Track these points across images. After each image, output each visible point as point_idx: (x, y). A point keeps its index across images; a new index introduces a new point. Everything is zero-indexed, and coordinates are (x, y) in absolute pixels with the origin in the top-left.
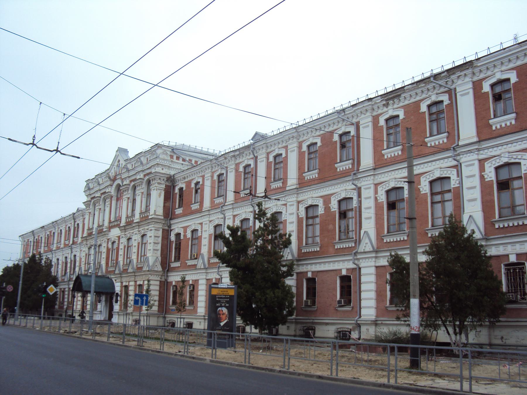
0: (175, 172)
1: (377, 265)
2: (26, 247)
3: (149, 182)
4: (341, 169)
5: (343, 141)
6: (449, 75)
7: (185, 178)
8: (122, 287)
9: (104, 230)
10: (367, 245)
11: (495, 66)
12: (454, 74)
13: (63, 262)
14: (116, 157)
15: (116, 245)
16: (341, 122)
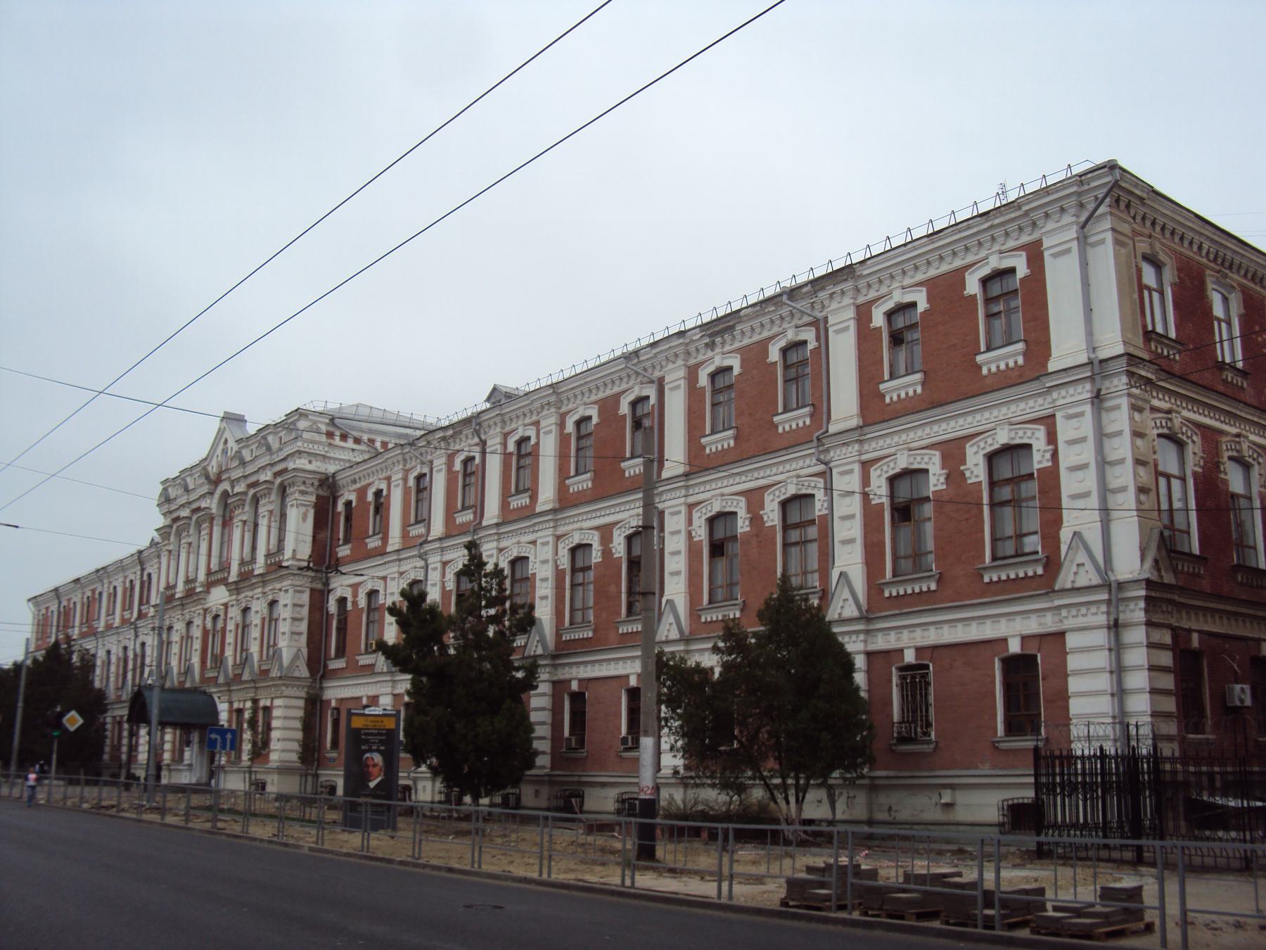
0: (339, 468)
1: (871, 647)
2: (42, 625)
3: (283, 490)
4: (787, 428)
5: (894, 328)
6: (815, 292)
7: (354, 482)
8: (231, 711)
9: (198, 590)
10: (847, 604)
11: (892, 277)
12: (823, 289)
13: (119, 659)
14: (220, 432)
15: (220, 624)
16: (633, 377)
